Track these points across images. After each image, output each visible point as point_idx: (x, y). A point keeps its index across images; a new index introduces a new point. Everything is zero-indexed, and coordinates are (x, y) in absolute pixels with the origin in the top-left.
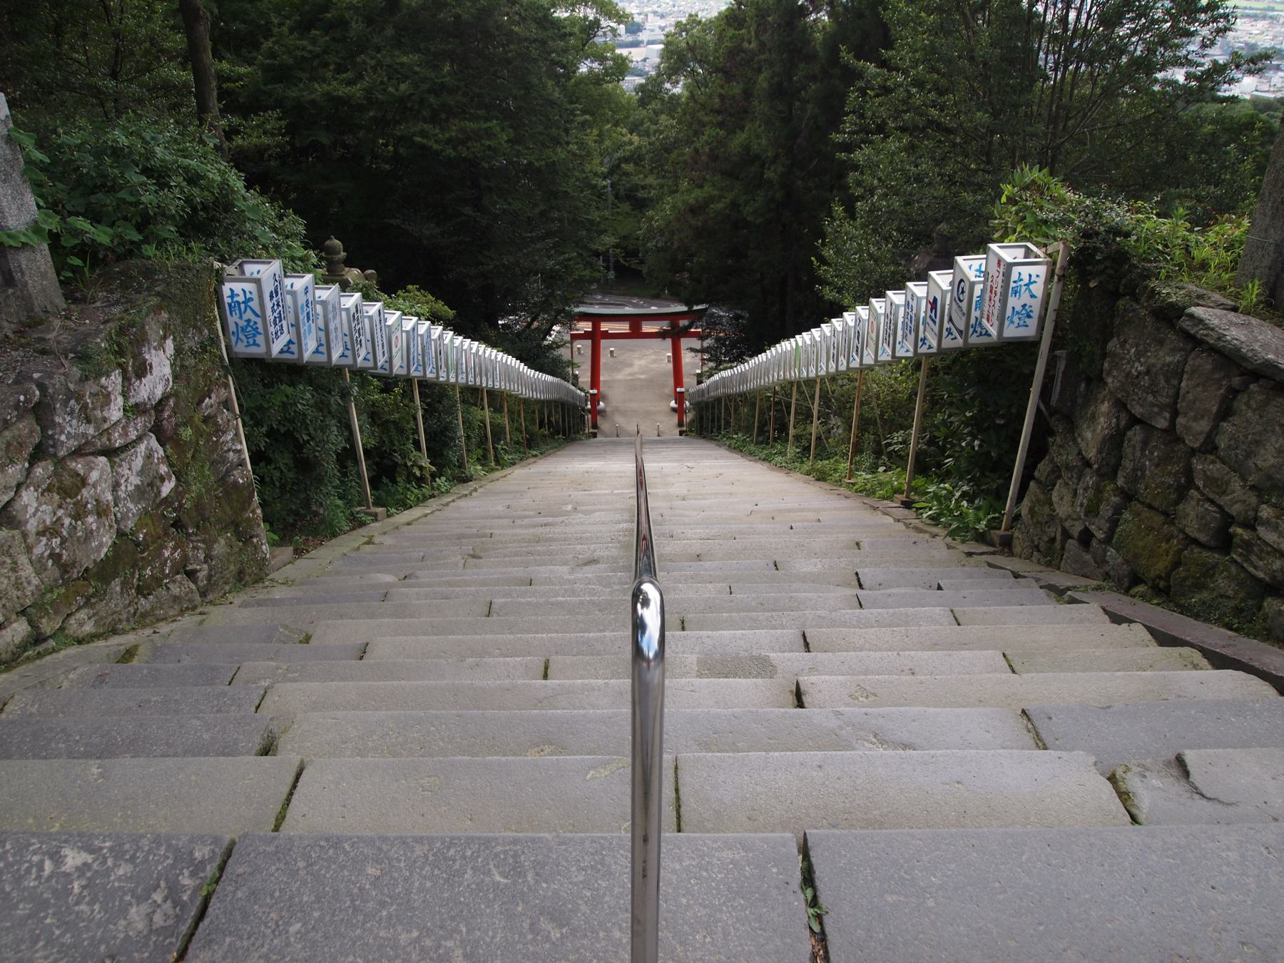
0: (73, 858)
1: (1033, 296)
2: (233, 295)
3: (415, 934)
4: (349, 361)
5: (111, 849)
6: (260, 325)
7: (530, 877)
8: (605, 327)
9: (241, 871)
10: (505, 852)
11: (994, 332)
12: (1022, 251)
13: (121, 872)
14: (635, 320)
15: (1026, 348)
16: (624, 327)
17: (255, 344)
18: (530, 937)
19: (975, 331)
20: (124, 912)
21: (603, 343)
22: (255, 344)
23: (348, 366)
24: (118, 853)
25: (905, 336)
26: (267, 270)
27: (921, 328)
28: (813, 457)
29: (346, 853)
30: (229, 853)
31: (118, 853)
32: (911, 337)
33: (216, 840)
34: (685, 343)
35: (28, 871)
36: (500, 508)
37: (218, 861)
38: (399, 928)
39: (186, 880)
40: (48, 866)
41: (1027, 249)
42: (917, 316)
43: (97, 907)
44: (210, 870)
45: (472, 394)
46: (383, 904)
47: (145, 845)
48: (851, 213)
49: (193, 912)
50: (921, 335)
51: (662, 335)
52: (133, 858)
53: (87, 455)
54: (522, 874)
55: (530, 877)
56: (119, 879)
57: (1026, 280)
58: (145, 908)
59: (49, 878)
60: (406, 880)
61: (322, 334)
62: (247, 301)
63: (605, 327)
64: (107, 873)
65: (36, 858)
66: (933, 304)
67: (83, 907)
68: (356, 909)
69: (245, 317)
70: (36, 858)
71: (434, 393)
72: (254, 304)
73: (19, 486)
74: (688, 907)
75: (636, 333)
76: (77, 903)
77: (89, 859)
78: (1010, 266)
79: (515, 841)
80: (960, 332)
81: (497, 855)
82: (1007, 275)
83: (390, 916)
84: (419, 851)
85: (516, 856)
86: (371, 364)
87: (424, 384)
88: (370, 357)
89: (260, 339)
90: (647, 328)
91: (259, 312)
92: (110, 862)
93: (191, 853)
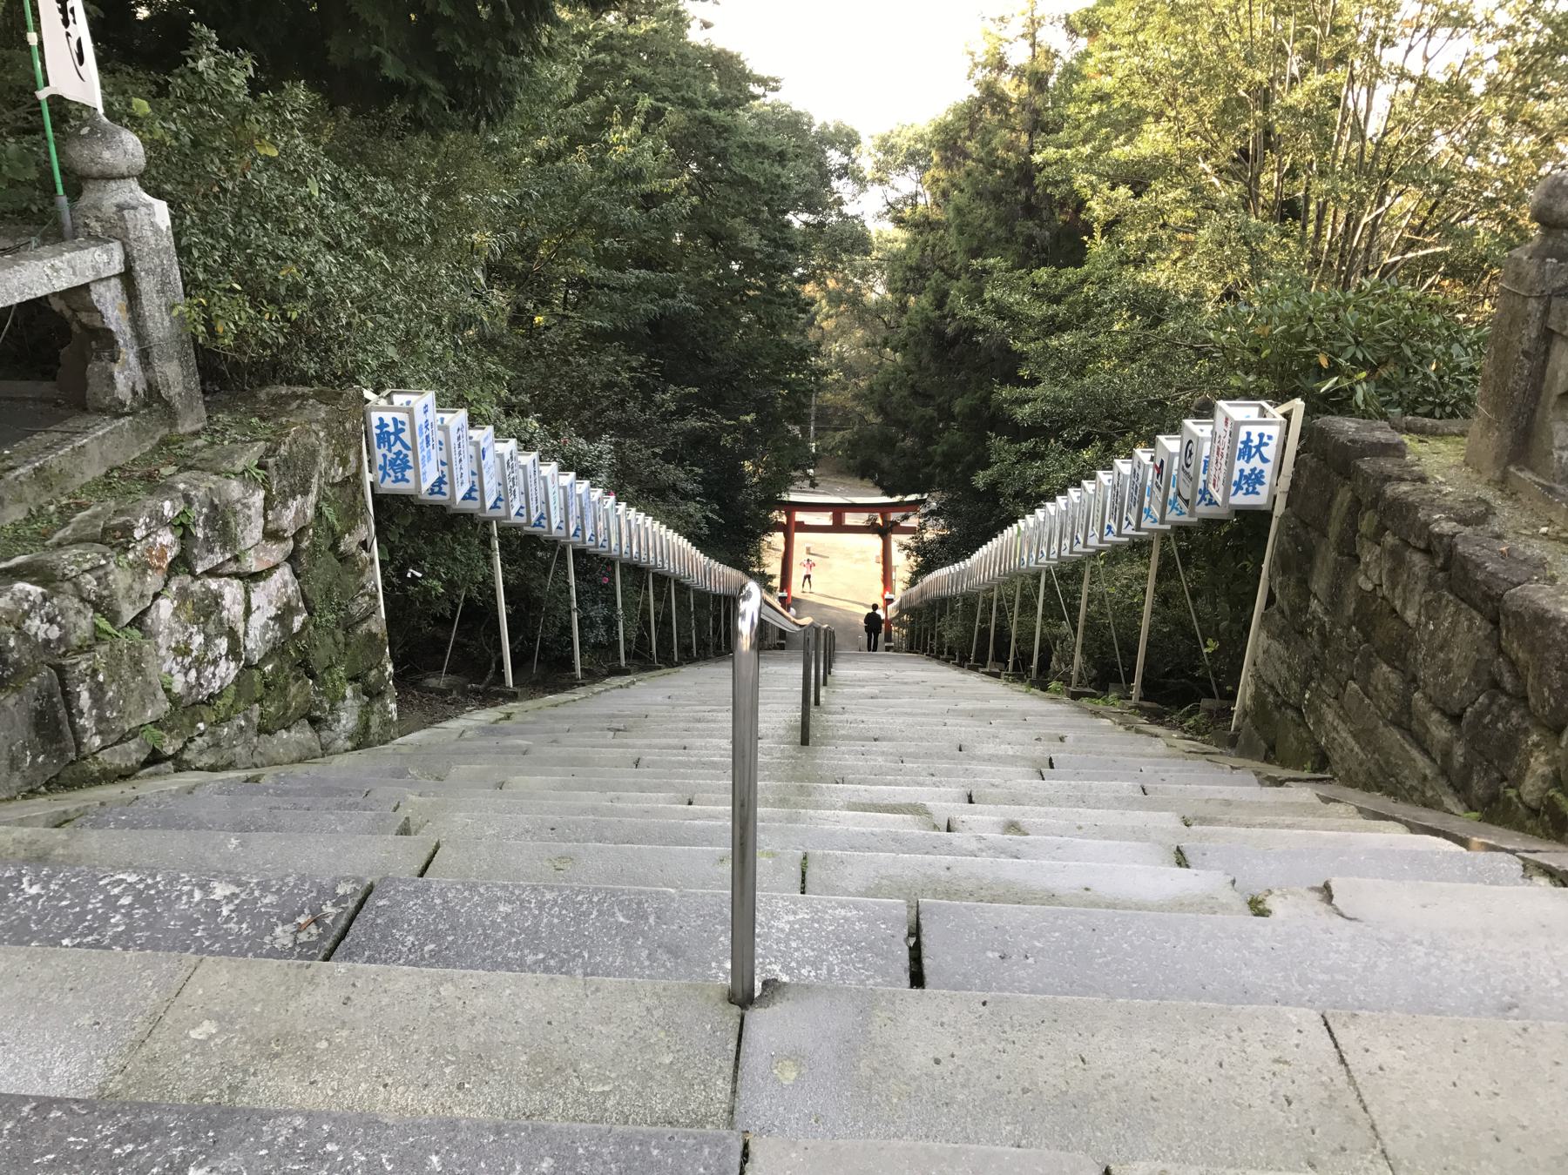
0: (220, 890)
1: (1264, 460)
2: (382, 425)
3: (541, 956)
4: (501, 513)
5: (258, 884)
6: (410, 458)
7: (652, 920)
8: (800, 516)
9: (381, 903)
10: (630, 901)
11: (1218, 497)
12: (1257, 410)
13: (267, 901)
14: (838, 510)
15: (1254, 520)
16: (825, 519)
17: (404, 479)
18: (647, 963)
19: (1203, 498)
20: (271, 929)
21: (799, 537)
22: (404, 479)
23: (498, 519)
24: (265, 887)
25: (1129, 509)
26: (422, 402)
27: (1147, 499)
28: (1028, 666)
29: (481, 895)
30: (370, 890)
31: (265, 887)
32: (1135, 510)
33: (358, 880)
34: (896, 539)
35: (179, 897)
36: (659, 699)
37: (359, 896)
38: (526, 951)
39: (328, 909)
40: (198, 895)
41: (1262, 408)
42: (1143, 485)
43: (244, 926)
44: (351, 905)
45: (636, 572)
46: (512, 933)
47: (291, 880)
48: (861, 182)
49: (336, 932)
50: (1146, 505)
51: (871, 528)
52: (279, 891)
53: (221, 576)
54: (645, 917)
55: (652, 920)
56: (266, 906)
57: (1256, 441)
58: (290, 928)
59: (198, 904)
60: (535, 917)
61: (476, 479)
62: (398, 431)
63: (800, 516)
64: (256, 900)
65: (186, 888)
66: (1159, 469)
67: (231, 925)
68: (487, 936)
69: (395, 449)
70: (186, 888)
71: (593, 565)
72: (406, 436)
73: (156, 596)
74: (797, 949)
75: (838, 527)
76: (226, 922)
77: (237, 891)
78: (1238, 425)
79: (640, 893)
80: (1187, 502)
81: (622, 902)
82: (1234, 435)
83: (518, 942)
84: (549, 896)
85: (640, 903)
86: (523, 520)
87: (580, 554)
88: (523, 511)
89: (409, 474)
90: (850, 519)
91: (409, 443)
92: (257, 893)
93: (334, 889)
